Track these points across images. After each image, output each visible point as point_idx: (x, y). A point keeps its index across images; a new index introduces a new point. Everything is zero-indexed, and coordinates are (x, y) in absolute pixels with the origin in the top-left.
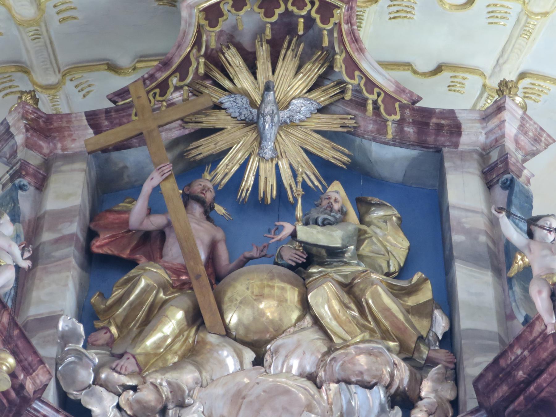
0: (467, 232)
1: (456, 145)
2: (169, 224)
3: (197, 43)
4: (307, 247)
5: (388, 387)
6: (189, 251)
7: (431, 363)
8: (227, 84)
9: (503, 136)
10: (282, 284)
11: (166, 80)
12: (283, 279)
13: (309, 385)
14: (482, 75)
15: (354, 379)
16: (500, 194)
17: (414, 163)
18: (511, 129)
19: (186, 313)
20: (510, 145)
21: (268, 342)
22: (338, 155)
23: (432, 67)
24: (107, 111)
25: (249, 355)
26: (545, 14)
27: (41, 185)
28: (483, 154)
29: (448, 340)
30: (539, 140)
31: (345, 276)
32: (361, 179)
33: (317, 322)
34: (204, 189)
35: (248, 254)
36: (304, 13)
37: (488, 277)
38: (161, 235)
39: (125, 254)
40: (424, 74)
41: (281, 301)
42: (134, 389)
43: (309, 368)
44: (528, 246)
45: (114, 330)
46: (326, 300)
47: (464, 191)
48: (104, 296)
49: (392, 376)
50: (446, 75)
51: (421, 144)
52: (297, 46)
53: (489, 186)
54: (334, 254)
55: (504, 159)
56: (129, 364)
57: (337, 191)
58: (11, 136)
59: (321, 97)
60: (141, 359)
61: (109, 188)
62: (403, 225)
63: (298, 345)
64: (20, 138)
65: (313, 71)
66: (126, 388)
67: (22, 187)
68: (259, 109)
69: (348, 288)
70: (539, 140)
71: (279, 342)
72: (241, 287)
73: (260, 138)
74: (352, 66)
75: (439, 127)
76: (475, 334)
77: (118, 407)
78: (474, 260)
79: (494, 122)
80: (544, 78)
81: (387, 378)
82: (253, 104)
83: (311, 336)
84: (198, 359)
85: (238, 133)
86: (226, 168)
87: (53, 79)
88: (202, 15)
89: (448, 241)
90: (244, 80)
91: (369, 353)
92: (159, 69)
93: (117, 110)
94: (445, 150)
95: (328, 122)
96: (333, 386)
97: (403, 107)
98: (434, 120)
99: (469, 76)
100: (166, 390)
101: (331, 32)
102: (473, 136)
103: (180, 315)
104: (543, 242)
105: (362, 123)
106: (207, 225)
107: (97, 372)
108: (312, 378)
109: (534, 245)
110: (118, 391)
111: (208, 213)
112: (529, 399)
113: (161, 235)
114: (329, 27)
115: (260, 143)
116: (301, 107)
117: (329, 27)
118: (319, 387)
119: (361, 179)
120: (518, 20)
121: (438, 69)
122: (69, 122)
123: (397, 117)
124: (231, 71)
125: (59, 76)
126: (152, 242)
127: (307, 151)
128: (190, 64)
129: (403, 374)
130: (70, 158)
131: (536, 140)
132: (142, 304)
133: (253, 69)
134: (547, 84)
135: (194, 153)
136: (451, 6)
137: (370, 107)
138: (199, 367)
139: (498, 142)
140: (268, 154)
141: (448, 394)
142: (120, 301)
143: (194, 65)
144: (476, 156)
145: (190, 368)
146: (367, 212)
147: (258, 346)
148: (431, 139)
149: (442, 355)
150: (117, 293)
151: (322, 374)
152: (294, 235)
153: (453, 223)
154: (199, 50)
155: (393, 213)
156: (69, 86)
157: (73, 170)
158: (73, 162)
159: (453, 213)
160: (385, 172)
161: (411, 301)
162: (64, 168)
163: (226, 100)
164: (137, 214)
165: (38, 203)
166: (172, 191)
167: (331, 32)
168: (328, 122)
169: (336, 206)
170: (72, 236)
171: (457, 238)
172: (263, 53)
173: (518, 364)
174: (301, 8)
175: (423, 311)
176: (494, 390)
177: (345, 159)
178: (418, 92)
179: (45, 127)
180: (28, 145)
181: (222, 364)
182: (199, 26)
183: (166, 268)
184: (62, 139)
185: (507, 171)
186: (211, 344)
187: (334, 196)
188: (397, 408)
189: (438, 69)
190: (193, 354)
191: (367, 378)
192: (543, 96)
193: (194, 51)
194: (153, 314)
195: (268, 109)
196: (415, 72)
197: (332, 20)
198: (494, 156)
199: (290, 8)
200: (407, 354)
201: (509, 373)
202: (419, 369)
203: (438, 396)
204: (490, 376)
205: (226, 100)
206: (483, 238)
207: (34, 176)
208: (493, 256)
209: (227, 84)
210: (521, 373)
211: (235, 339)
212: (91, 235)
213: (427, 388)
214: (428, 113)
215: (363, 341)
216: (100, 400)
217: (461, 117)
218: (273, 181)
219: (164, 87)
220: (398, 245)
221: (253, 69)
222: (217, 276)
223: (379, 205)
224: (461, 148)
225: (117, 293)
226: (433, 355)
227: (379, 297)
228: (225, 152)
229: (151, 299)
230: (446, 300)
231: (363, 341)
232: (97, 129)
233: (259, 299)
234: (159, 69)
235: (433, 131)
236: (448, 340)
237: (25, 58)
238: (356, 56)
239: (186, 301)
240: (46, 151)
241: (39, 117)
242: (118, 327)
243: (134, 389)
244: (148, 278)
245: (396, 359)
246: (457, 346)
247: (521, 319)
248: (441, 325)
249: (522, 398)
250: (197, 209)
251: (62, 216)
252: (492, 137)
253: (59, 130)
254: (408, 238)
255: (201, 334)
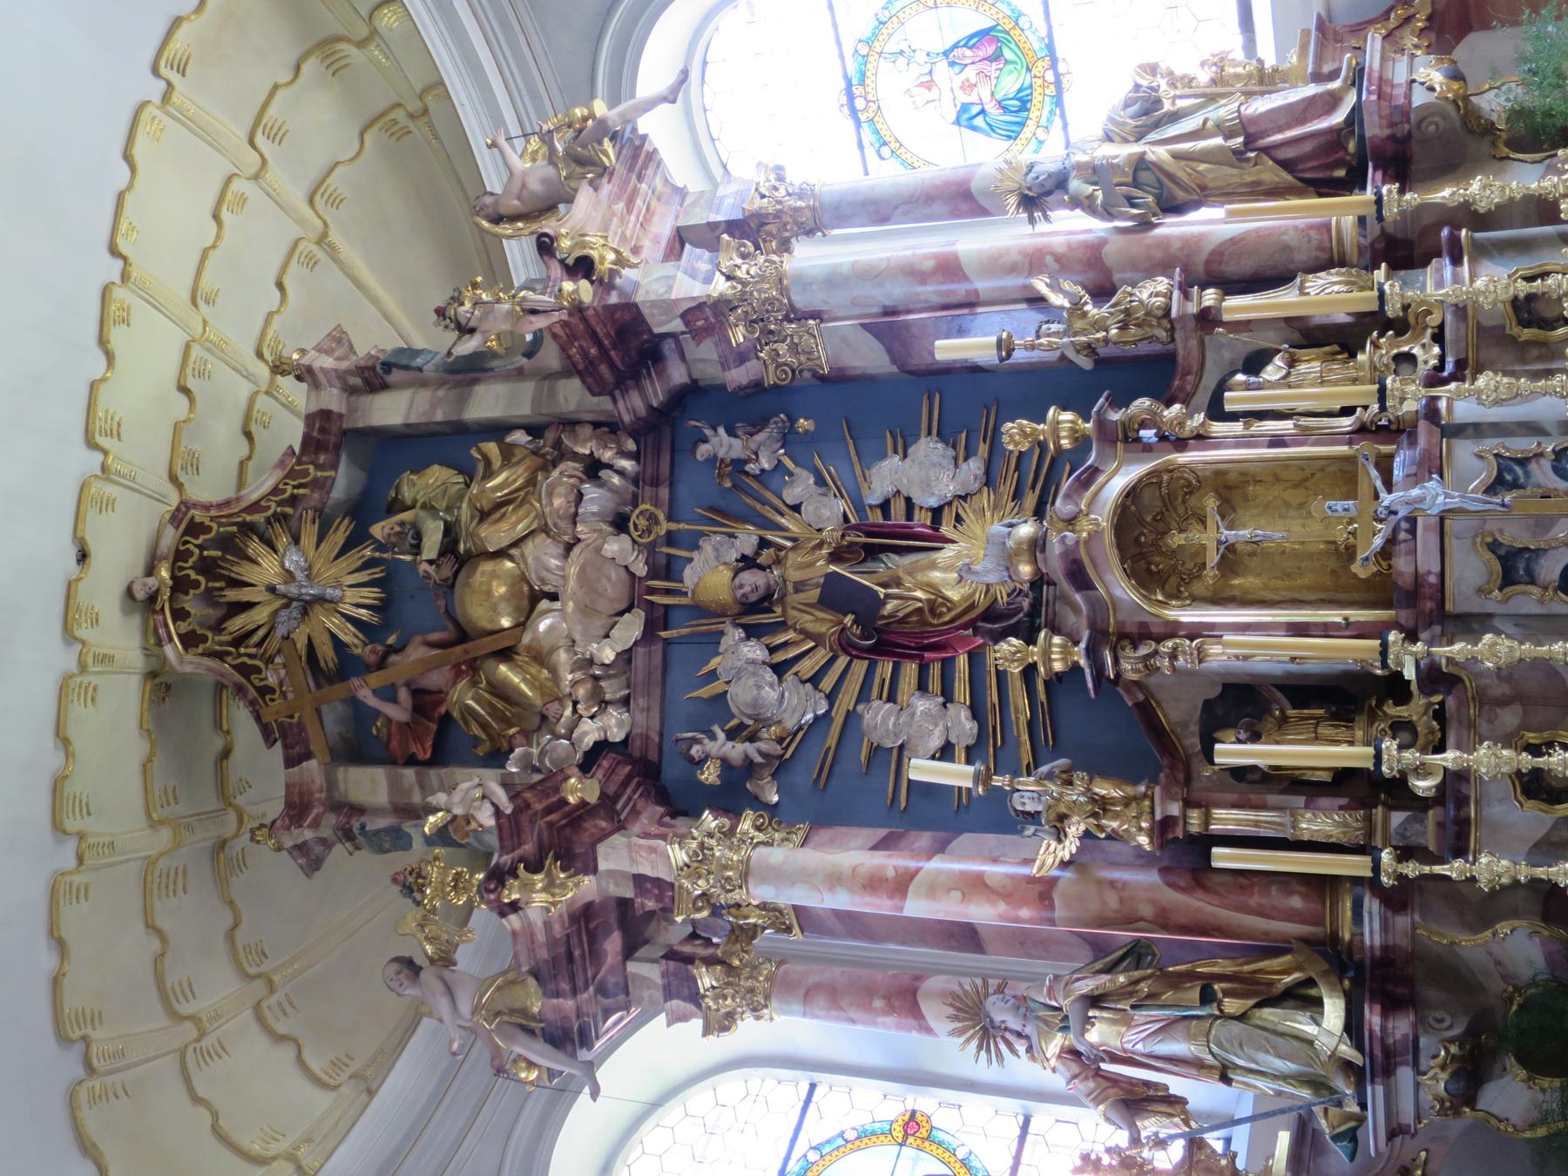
0: (434, 407)
1: (341, 416)
2: (407, 684)
3: (220, 656)
4: (441, 554)
5: (582, 481)
6: (430, 666)
7: (558, 444)
8: (261, 633)
9: (336, 371)
10: (478, 574)
11: (257, 689)
12: (470, 576)
13: (576, 550)
14: (257, 393)
15: (573, 510)
16: (395, 376)
17: (353, 460)
18: (327, 362)
19: (502, 661)
20: (344, 365)
21: (531, 588)
22: (342, 528)
23: (245, 442)
24: (286, 747)
25: (544, 604)
26: (205, 323)
27: (358, 810)
28: (352, 391)
29: (534, 430)
30: (338, 339)
31: (472, 518)
32: (362, 511)
33: (516, 544)
34: (373, 651)
35: (442, 610)
36: (197, 551)
37: (480, 389)
38: (418, 693)
39: (434, 727)
40: (252, 450)
41: (494, 575)
42: (575, 703)
43: (560, 550)
44: (484, 333)
45: (512, 731)
46: (495, 535)
47: (390, 410)
48: (477, 741)
49: (571, 476)
50: (254, 428)
51: (337, 449)
52: (227, 561)
53: (385, 387)
54: (450, 531)
55: (360, 370)
56: (553, 708)
57: (379, 530)
58: (305, 843)
59: (283, 540)
60: (547, 699)
61: (358, 747)
62: (418, 469)
63: (537, 559)
64: (308, 835)
65: (255, 547)
66: (575, 711)
67: (363, 827)
68: (291, 600)
69: (484, 515)
70: (338, 339)
71: (533, 577)
72: (476, 613)
73: (321, 600)
74: (255, 507)
75: (322, 430)
76: (536, 401)
77: (592, 717)
78: (462, 401)
79: (322, 379)
80: (263, 334)
81: (572, 481)
82: (287, 606)
83: (529, 548)
84: (546, 650)
85: (314, 621)
86: (348, 635)
87: (232, 817)
88: (192, 650)
89: (438, 428)
90: (260, 616)
91: (550, 494)
92: (245, 696)
93: (284, 736)
94: (345, 426)
95: (309, 534)
96: (579, 528)
97: (299, 463)
98: (315, 434)
99: (257, 406)
100: (579, 675)
101: (220, 525)
102: (333, 399)
103: (503, 668)
104: (480, 319)
105: (312, 504)
106: (409, 650)
107: (557, 737)
108: (569, 548)
109: (484, 327)
110: (577, 718)
111: (399, 649)
112: (614, 347)
113: (418, 693)
114: (215, 526)
115: (326, 601)
116: (293, 560)
117: (215, 526)
118: (579, 540)
119: (362, 511)
120: (208, 350)
121: (248, 435)
122: (294, 785)
123: (311, 468)
124: (251, 627)
125: (230, 810)
126: (424, 701)
127: (336, 558)
128: (243, 664)
129: (569, 466)
130: (331, 783)
131: (339, 341)
132: (491, 705)
133: (250, 605)
134: (270, 333)
135: (331, 665)
136: (190, 411)
137: (301, 491)
138: (554, 650)
139: (341, 376)
140: (338, 592)
141: (587, 430)
142: (484, 726)
143: (245, 659)
144: (353, 398)
145: (554, 657)
146: (403, 502)
147: (533, 598)
148: (333, 439)
149: (550, 435)
150: (476, 730)
151: (566, 538)
152: (431, 562)
153: (423, 420)
154: (229, 653)
155: (407, 476)
156: (240, 800)
157: (346, 781)
158: (336, 781)
159: (413, 419)
160: (358, 488)
161: (497, 463)
162: (342, 788)
163: (281, 631)
164: (398, 712)
165: (378, 812)
166: (376, 679)
167: (220, 525)
168: (309, 534)
169: (398, 529)
170: (417, 774)
171: (439, 416)
172: (232, 595)
173: (584, 353)
174: (191, 554)
175: (508, 452)
176: (601, 377)
177: (346, 521)
178: (283, 449)
179: (297, 808)
180: (315, 825)
181: (551, 629)
182: (202, 655)
183: (455, 683)
184: (311, 793)
185: (373, 368)
186: (533, 640)
187: (387, 530)
188: (601, 474)
189: (248, 435)
190: (541, 657)
191: (572, 498)
192: (281, 338)
193: (229, 659)
194: (500, 691)
195: (293, 590)
196: (249, 458)
197: (207, 522)
198: (356, 381)
199: (190, 564)
200: (548, 465)
201: (590, 363)
202: (562, 454)
203: (590, 439)
204: (590, 380)
205: (281, 631)
206: (441, 393)
207: (349, 817)
208: (458, 385)
209: (261, 633)
210: (593, 351)
211: (528, 618)
212: (411, 761)
213: (584, 450)
214: (307, 440)
215: (540, 501)
216: (585, 734)
217: (313, 408)
218: (365, 591)
219: (265, 691)
220: (437, 475)
221: (250, 605)
222: (463, 634)
223: (398, 489)
224: (344, 411)
225: (476, 730)
226: (549, 443)
227: (501, 482)
228: (333, 637)
229: (487, 696)
230: (497, 430)
231: (540, 501)
232: (308, 756)
233: (489, 598)
234: (245, 696)
235: (324, 436)
236: (534, 430)
237: (209, 843)
238: (244, 504)
239: (490, 663)
240: (321, 809)
241: (288, 814)
242: (511, 726)
243: (575, 703)
244: (465, 697)
245: (555, 474)
246: (543, 419)
247: (525, 360)
248: (519, 437)
249: (612, 353)
250: (394, 658)
251: (395, 786)
252: (336, 381)
253: (301, 794)
254: (427, 466)
255: (521, 649)
